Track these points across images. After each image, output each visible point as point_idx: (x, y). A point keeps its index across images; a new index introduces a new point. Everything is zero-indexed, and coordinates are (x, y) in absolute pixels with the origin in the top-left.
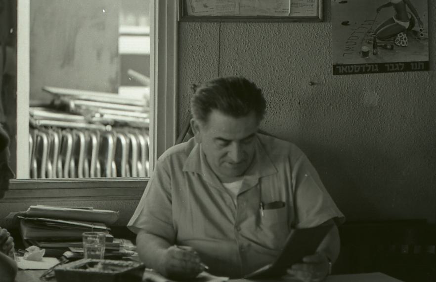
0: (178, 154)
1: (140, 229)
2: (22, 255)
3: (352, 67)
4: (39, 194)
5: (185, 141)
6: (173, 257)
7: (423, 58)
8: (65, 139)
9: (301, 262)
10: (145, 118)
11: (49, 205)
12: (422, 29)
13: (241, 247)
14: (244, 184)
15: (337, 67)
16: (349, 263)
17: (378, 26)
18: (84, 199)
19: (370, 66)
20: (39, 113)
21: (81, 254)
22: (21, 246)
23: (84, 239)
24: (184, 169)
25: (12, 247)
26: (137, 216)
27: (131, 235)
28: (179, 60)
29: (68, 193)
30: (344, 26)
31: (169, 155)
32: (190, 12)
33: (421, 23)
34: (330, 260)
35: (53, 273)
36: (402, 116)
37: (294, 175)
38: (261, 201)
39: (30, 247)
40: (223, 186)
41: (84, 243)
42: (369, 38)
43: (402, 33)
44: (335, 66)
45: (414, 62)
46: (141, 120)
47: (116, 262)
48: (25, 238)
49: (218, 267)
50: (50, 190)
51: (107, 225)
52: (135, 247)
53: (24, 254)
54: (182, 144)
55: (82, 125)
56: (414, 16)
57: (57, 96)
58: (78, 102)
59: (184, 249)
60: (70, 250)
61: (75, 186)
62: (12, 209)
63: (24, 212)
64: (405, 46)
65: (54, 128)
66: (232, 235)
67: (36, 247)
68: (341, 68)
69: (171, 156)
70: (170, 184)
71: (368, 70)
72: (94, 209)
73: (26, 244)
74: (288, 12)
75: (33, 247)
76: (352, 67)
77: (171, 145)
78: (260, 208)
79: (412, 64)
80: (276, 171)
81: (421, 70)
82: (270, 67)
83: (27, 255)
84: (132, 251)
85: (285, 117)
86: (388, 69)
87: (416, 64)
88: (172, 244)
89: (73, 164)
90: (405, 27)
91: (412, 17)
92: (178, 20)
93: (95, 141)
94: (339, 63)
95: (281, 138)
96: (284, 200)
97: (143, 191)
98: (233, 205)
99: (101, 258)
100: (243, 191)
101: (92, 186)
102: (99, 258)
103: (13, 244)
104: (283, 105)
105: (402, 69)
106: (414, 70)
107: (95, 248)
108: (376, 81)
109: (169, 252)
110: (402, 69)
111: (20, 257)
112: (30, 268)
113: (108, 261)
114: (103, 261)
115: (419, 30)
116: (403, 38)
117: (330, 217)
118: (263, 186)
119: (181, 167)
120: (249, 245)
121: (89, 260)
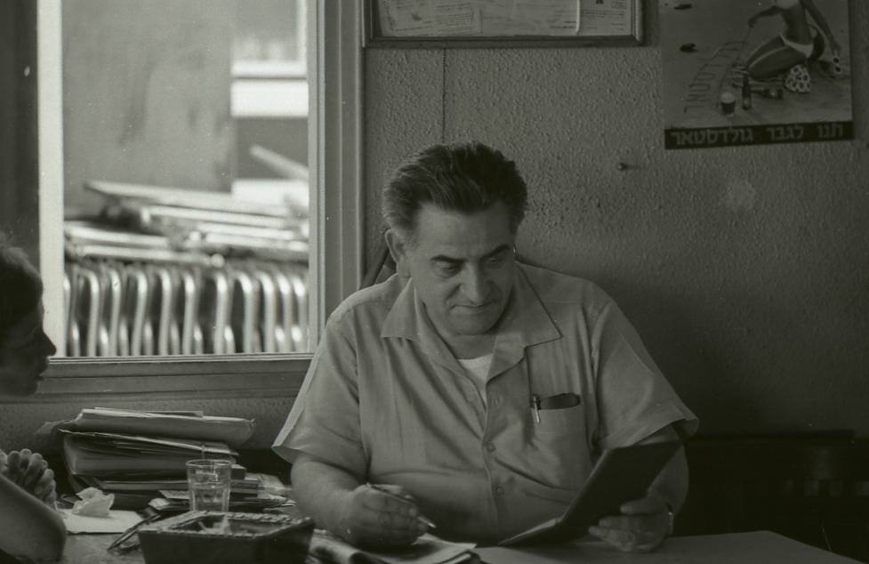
0: (369, 305)
1: (298, 452)
2: (70, 506)
3: (703, 133)
4: (96, 386)
5: (380, 282)
6: (365, 507)
7: (841, 114)
8: (132, 284)
9: (618, 513)
12: (839, 58)
13: (496, 486)
14: (497, 360)
15: (673, 134)
16: (706, 515)
17: (752, 53)
19: (737, 132)
20: (82, 232)
22: (68, 489)
23: (189, 474)
24: (383, 335)
25: (51, 490)
26: (292, 428)
27: (280, 468)
29: (153, 384)
30: (684, 54)
31: (351, 307)
32: (387, 30)
33: (835, 46)
35: (135, 539)
38: (532, 394)
39: (86, 491)
40: (460, 364)
41: (189, 481)
42: (735, 76)
43: (798, 67)
44: (668, 132)
45: (823, 124)
46: (280, 246)
47: (256, 516)
48: (74, 473)
49: (452, 521)
50: (119, 379)
51: (231, 447)
52: (289, 489)
53: (73, 505)
54: (375, 286)
56: (822, 32)
57: (114, 199)
58: (157, 211)
59: (385, 491)
60: (162, 497)
61: (167, 370)
62: (47, 415)
63: (71, 421)
64: (806, 93)
66: (479, 461)
67: (96, 489)
68: (681, 136)
69: (355, 308)
71: (734, 140)
73: (75, 485)
74: (573, 27)
75: (91, 490)
78: (532, 406)
80: (558, 334)
81: (837, 138)
82: (542, 134)
83: (79, 506)
84: (282, 496)
85: (573, 232)
86: (773, 137)
87: (827, 127)
88: (364, 482)
89: (148, 332)
90: (804, 55)
91: (819, 35)
92: (364, 45)
93: (191, 287)
94: (677, 125)
95: (566, 273)
96: (578, 391)
98: (480, 402)
99: (223, 509)
101: (199, 370)
102: (220, 510)
103: (53, 483)
104: (567, 209)
105: (799, 137)
106: (824, 139)
107: (212, 490)
108: (749, 161)
109: (359, 498)
110: (799, 137)
112: (87, 531)
113: (239, 515)
114: (230, 514)
116: (802, 76)
117: (669, 422)
119: (376, 330)
120: (511, 481)
121: (202, 514)
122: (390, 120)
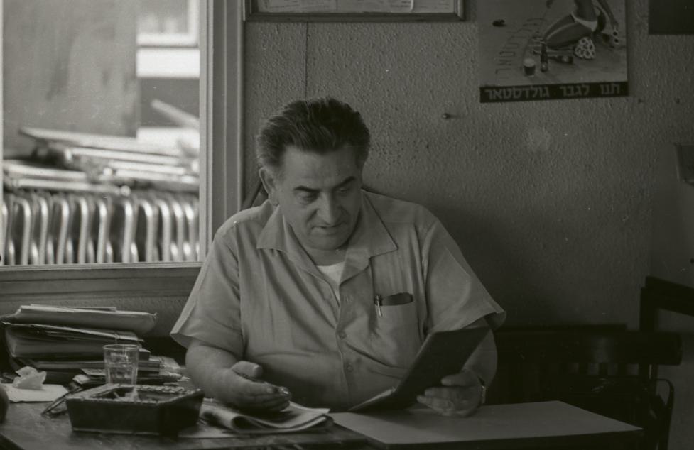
0: (247, 223)
1: (191, 339)
2: (11, 381)
3: (510, 90)
8: (57, 209)
9: (439, 385)
10: (194, 174)
11: (48, 304)
12: (617, 32)
13: (347, 366)
15: (487, 91)
16: (510, 388)
18: (95, 296)
19: (536, 89)
20: (17, 168)
21: (101, 378)
24: (258, 247)
27: (177, 351)
28: (245, 80)
33: (614, 23)
34: (483, 383)
35: (63, 406)
36: (586, 166)
37: (425, 253)
38: (375, 294)
40: (317, 269)
41: (106, 361)
43: (585, 39)
44: (483, 90)
45: (605, 83)
46: (174, 179)
48: (14, 356)
50: (50, 282)
51: (138, 336)
53: (13, 381)
55: (84, 187)
56: (604, 11)
57: (43, 142)
58: (77, 151)
61: (88, 275)
63: (11, 316)
64: (591, 59)
65: (40, 192)
66: (333, 345)
67: (31, 368)
68: (493, 93)
69: (237, 226)
70: (238, 270)
71: (534, 96)
72: (118, 309)
74: (409, 6)
75: (28, 368)
76: (510, 90)
77: (234, 212)
78: (375, 303)
79: (602, 87)
81: (615, 95)
83: (17, 381)
85: (407, 168)
86: (565, 94)
87: (608, 86)
89: (70, 248)
91: (601, 13)
92: (244, 19)
93: (104, 212)
95: (402, 199)
96: (411, 291)
97: (193, 283)
100: (349, 277)
105: (586, 94)
106: (605, 96)
107: (124, 369)
108: (546, 113)
111: (7, 385)
113: (145, 387)
114: (137, 387)
115: (612, 34)
116: (588, 46)
118: (377, 270)
119: (254, 243)
120: (359, 361)
121: (116, 386)
122: (264, 78)
